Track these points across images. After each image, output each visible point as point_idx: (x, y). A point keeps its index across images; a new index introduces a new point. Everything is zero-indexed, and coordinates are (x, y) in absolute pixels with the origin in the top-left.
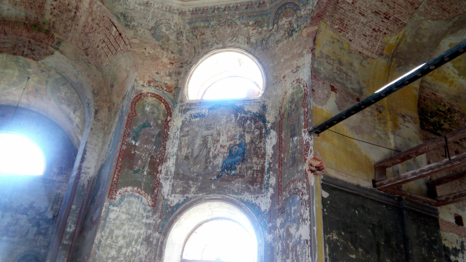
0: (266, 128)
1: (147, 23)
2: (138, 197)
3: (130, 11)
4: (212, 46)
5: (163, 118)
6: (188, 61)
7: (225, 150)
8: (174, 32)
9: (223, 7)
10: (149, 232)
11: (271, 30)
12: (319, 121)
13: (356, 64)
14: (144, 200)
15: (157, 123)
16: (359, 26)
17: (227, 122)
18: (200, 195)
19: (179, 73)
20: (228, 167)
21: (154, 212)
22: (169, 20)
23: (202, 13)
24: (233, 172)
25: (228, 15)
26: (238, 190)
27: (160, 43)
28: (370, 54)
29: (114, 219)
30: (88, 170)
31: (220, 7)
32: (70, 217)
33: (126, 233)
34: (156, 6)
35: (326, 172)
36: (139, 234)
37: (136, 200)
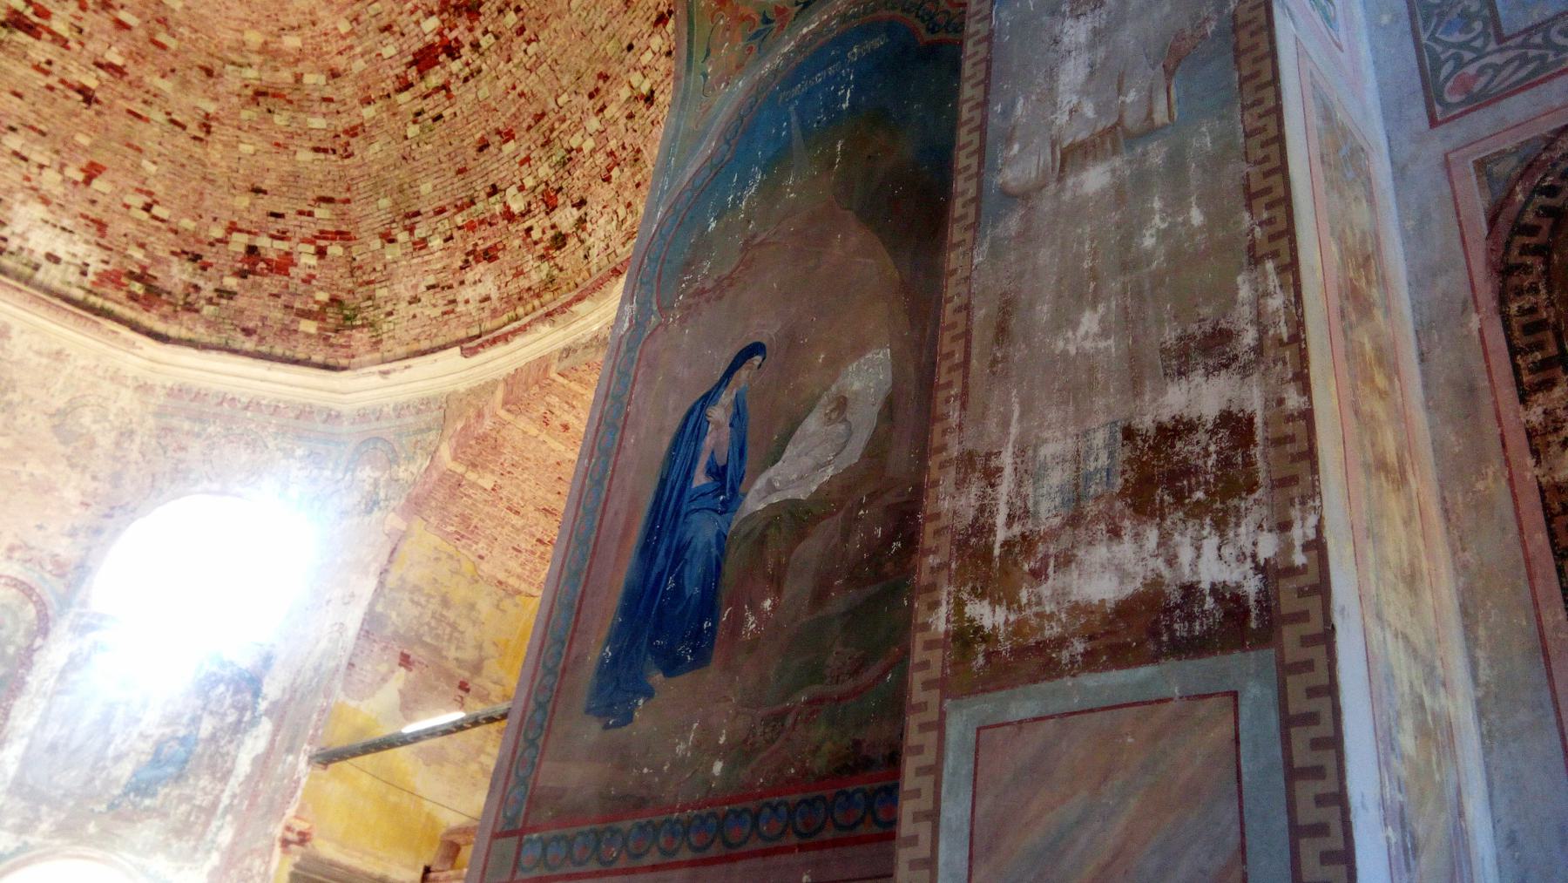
0: (254, 709)
3: (9, 365)
4: (197, 481)
5: (20, 639)
6: (128, 503)
7: (147, 747)
9: (245, 400)
11: (338, 481)
12: (341, 737)
13: (485, 606)
16: (505, 531)
18: (58, 842)
19: (98, 531)
20: (141, 788)
22: (106, 399)
23: (191, 400)
25: (252, 420)
27: (69, 451)
28: (523, 587)
31: (237, 397)
34: (81, 362)
35: (313, 847)
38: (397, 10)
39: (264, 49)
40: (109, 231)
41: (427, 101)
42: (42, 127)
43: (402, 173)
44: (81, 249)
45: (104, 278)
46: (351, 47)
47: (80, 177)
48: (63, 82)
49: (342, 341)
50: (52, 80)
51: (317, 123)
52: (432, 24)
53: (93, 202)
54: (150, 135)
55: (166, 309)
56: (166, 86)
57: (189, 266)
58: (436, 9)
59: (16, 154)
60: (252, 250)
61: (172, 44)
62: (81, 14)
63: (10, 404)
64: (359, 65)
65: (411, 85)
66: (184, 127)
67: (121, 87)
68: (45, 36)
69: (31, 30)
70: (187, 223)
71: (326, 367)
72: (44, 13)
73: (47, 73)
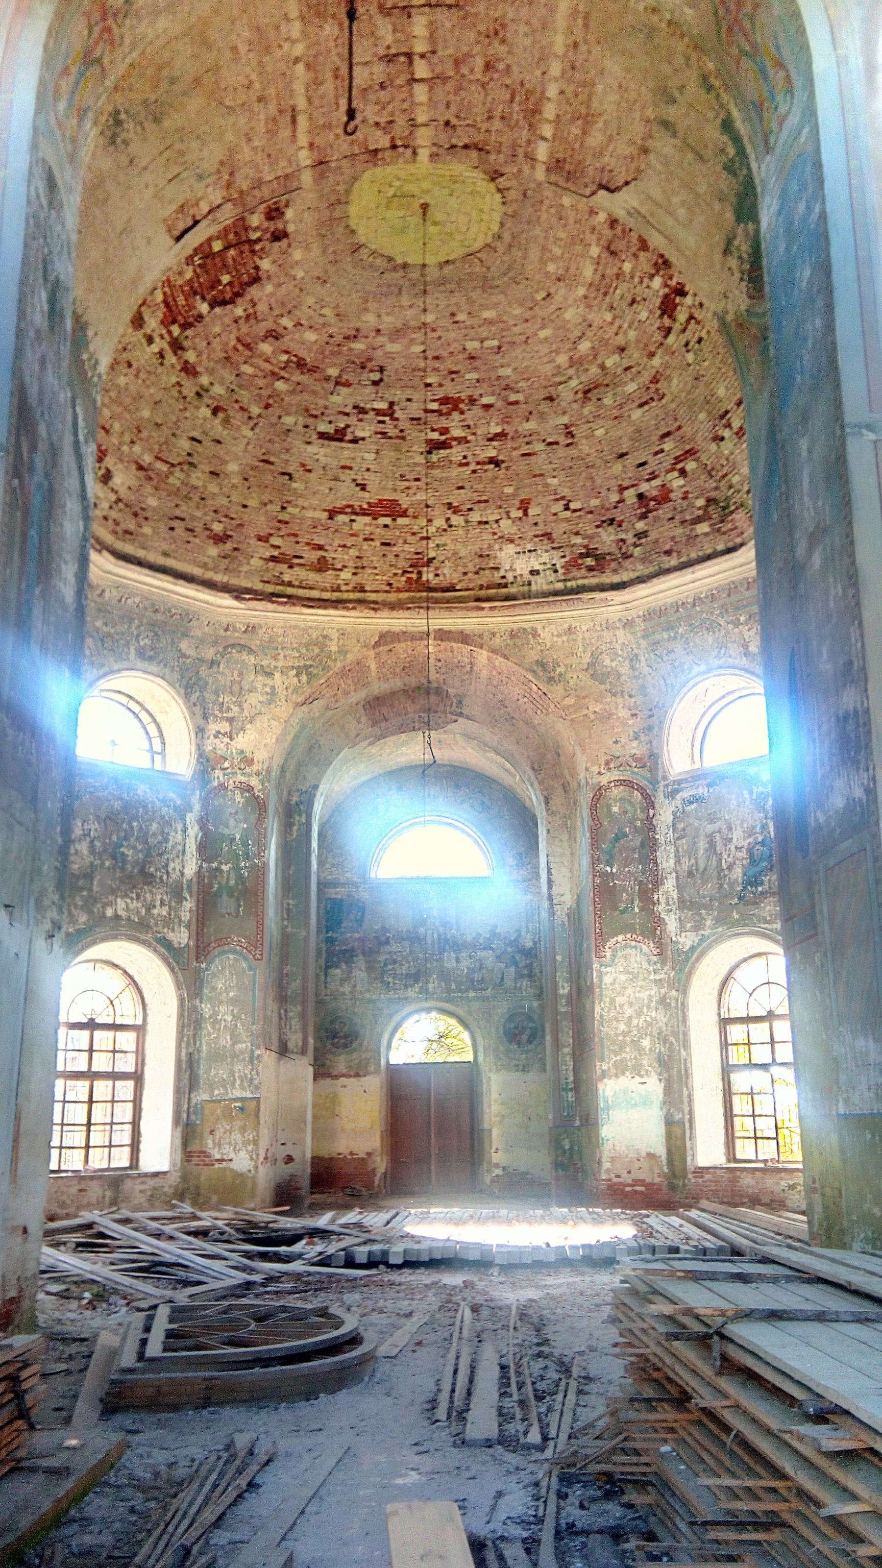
5: (640, 815)
7: (743, 854)
9: (690, 600)
10: (663, 991)
14: (644, 948)
19: (650, 729)
20: (752, 881)
21: (664, 963)
33: (632, 999)
34: (584, 628)
37: (634, 951)
39: (572, 363)
40: (554, 536)
41: (688, 332)
43: (701, 390)
44: (545, 557)
45: (567, 567)
46: (620, 327)
47: (520, 514)
48: (478, 463)
49: (730, 526)
50: (473, 467)
51: (631, 387)
52: (657, 282)
53: (536, 524)
55: (613, 565)
56: (532, 425)
57: (611, 529)
59: (480, 523)
60: (640, 496)
61: (520, 397)
63: (560, 675)
64: (632, 334)
66: (557, 443)
67: (510, 444)
70: (595, 502)
73: (467, 464)
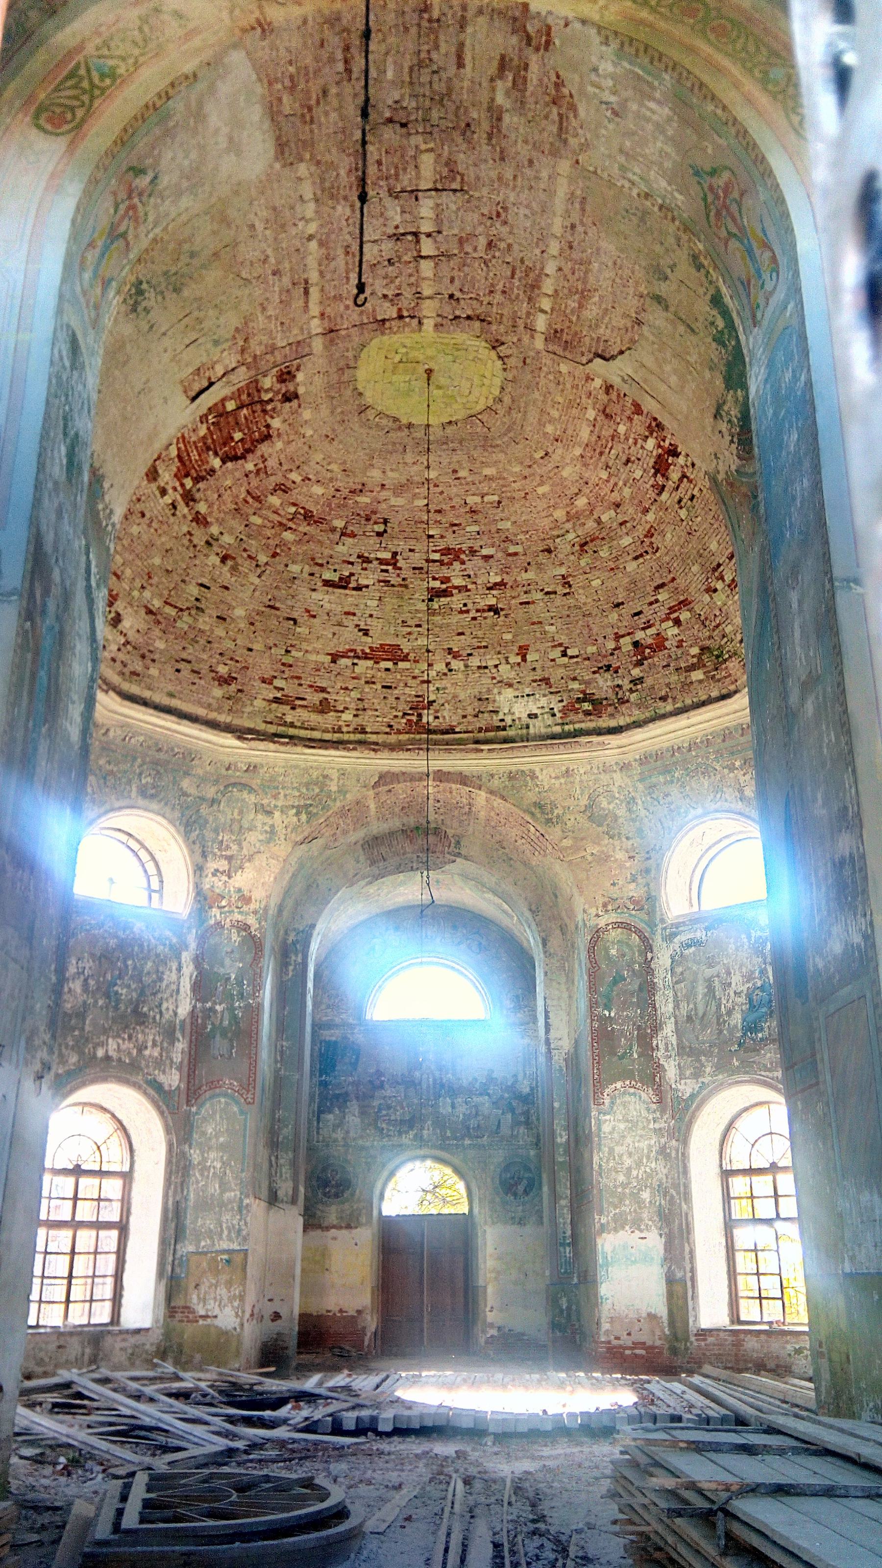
1: (576, 803)
2: (634, 1094)
7: (742, 1000)
8: (622, 801)
10: (663, 1141)
15: (633, 970)
17: (737, 949)
18: (720, 1077)
19: (648, 871)
21: (663, 1111)
24: (760, 1035)
26: (771, 1064)
27: (605, 828)
29: (610, 1133)
30: (560, 1043)
32: (556, 1122)
33: (631, 1149)
36: (650, 1147)
38: (626, 447)
42: (484, 644)
44: (543, 701)
45: (565, 711)
46: (616, 484)
47: (519, 659)
48: (478, 611)
49: (723, 673)
50: (473, 614)
52: (651, 443)
53: (534, 669)
54: (539, 610)
55: (610, 709)
56: (531, 575)
57: (607, 675)
58: (647, 434)
59: (479, 667)
60: (636, 644)
61: (519, 549)
62: (463, 567)
64: (627, 492)
65: (664, 487)
66: (555, 593)
67: (509, 593)
68: (455, 591)
69: (445, 593)
70: (592, 649)
71: (723, 697)
72: (445, 580)
73: (468, 612)
